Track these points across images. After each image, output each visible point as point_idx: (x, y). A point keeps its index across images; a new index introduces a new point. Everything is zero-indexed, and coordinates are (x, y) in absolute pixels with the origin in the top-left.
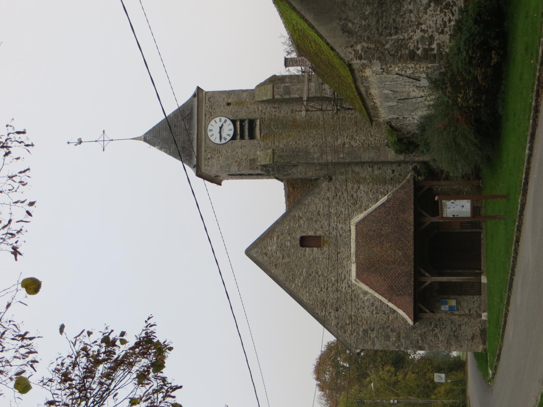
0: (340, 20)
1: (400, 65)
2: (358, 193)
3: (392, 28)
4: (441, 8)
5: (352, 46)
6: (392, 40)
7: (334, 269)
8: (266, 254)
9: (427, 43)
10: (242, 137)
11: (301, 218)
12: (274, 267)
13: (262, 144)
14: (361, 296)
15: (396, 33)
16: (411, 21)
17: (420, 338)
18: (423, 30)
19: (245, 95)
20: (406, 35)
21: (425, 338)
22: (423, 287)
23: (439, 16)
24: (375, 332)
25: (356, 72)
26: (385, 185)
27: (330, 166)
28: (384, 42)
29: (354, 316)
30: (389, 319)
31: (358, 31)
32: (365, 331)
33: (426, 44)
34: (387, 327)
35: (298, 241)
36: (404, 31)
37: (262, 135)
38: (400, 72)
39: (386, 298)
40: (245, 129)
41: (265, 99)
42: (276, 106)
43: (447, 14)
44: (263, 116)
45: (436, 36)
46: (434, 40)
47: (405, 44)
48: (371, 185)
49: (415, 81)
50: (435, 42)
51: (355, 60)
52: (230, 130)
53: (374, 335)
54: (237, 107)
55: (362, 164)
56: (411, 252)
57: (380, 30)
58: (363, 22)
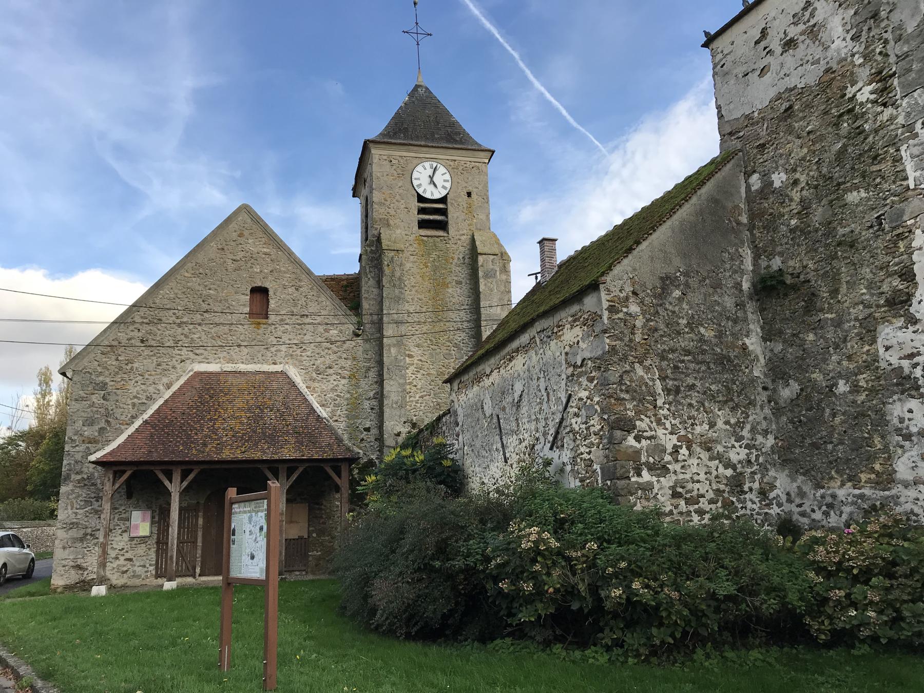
0: (686, 274)
1: (596, 399)
2: (334, 377)
3: (676, 383)
4: (724, 491)
5: (635, 293)
7: (213, 338)
8: (241, 235)
10: (421, 211)
11: (297, 290)
12: (220, 247)
13: (412, 238)
14: (165, 380)
15: (667, 391)
16: (692, 425)
17: (85, 477)
20: (666, 412)
21: (85, 485)
22: (162, 477)
23: (707, 487)
24: (102, 401)
25: (575, 308)
26: (347, 417)
27: (378, 335)
28: (647, 363)
29: (132, 369)
30: (122, 424)
31: (666, 310)
32: (104, 386)
33: (648, 456)
34: (108, 422)
35: (260, 284)
36: (673, 408)
37: (425, 238)
39: (152, 416)
40: (433, 216)
41: (477, 243)
42: (467, 261)
43: (713, 506)
44: (453, 241)
45: (667, 482)
46: (658, 476)
47: (647, 409)
48: (348, 396)
50: (655, 479)
51: (608, 298)
52: (432, 194)
53: (95, 401)
55: (380, 382)
56: (227, 454)
57: (670, 356)
58: (685, 322)
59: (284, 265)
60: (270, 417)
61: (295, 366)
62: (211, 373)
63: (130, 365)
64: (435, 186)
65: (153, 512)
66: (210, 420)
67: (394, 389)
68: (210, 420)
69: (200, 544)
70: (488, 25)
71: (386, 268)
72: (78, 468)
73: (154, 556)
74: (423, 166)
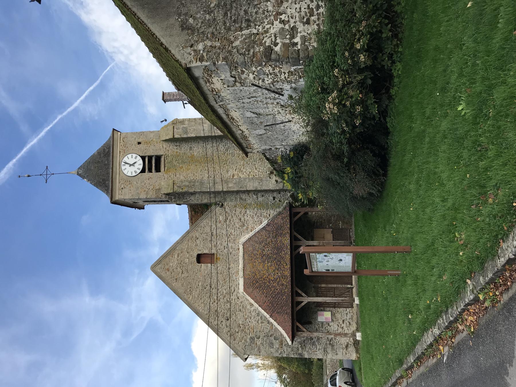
0: (180, 15)
1: (254, 69)
2: (245, 217)
3: (244, 22)
5: (192, 46)
6: (242, 35)
7: (225, 283)
8: (168, 270)
9: (288, 37)
10: (150, 170)
11: (198, 239)
13: (166, 176)
14: (248, 307)
15: (248, 27)
18: (283, 21)
19: (152, 135)
20: (260, 28)
24: (260, 339)
25: (202, 82)
26: (267, 209)
28: (232, 39)
29: (243, 324)
30: (272, 328)
31: (201, 27)
32: (252, 339)
33: (286, 38)
34: (271, 336)
35: (195, 259)
37: (166, 168)
38: (256, 82)
39: (267, 313)
40: (152, 164)
41: (167, 138)
44: (167, 152)
45: (301, 27)
46: (297, 33)
47: (259, 39)
49: (277, 96)
50: (299, 35)
51: (194, 62)
52: (140, 164)
54: (146, 145)
55: (248, 192)
56: (288, 273)
57: (228, 25)
58: (207, 16)
59: (184, 246)
60: (268, 251)
61: (240, 238)
62: (244, 283)
63: (241, 325)
64: (135, 163)
65: (318, 310)
66: (269, 282)
67: (251, 184)
68: (269, 282)
69: (335, 286)
70: (43, 134)
71: (184, 190)
72: (295, 349)
73: (341, 309)
74: (124, 170)
